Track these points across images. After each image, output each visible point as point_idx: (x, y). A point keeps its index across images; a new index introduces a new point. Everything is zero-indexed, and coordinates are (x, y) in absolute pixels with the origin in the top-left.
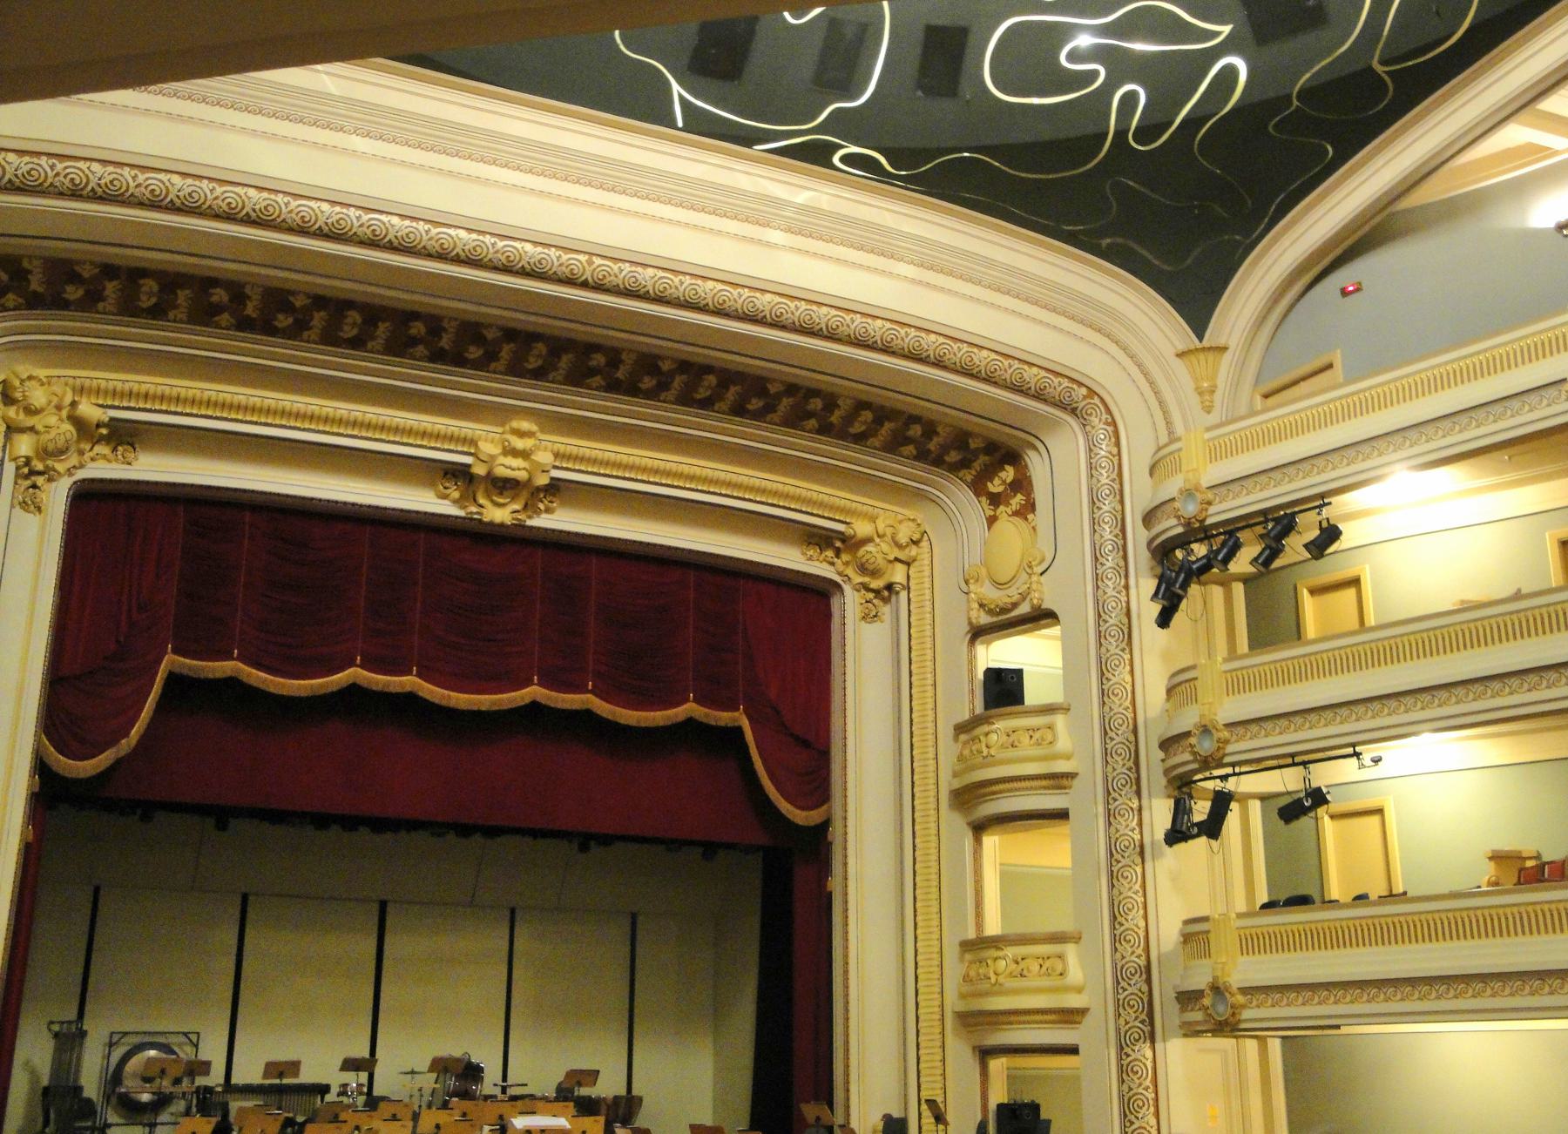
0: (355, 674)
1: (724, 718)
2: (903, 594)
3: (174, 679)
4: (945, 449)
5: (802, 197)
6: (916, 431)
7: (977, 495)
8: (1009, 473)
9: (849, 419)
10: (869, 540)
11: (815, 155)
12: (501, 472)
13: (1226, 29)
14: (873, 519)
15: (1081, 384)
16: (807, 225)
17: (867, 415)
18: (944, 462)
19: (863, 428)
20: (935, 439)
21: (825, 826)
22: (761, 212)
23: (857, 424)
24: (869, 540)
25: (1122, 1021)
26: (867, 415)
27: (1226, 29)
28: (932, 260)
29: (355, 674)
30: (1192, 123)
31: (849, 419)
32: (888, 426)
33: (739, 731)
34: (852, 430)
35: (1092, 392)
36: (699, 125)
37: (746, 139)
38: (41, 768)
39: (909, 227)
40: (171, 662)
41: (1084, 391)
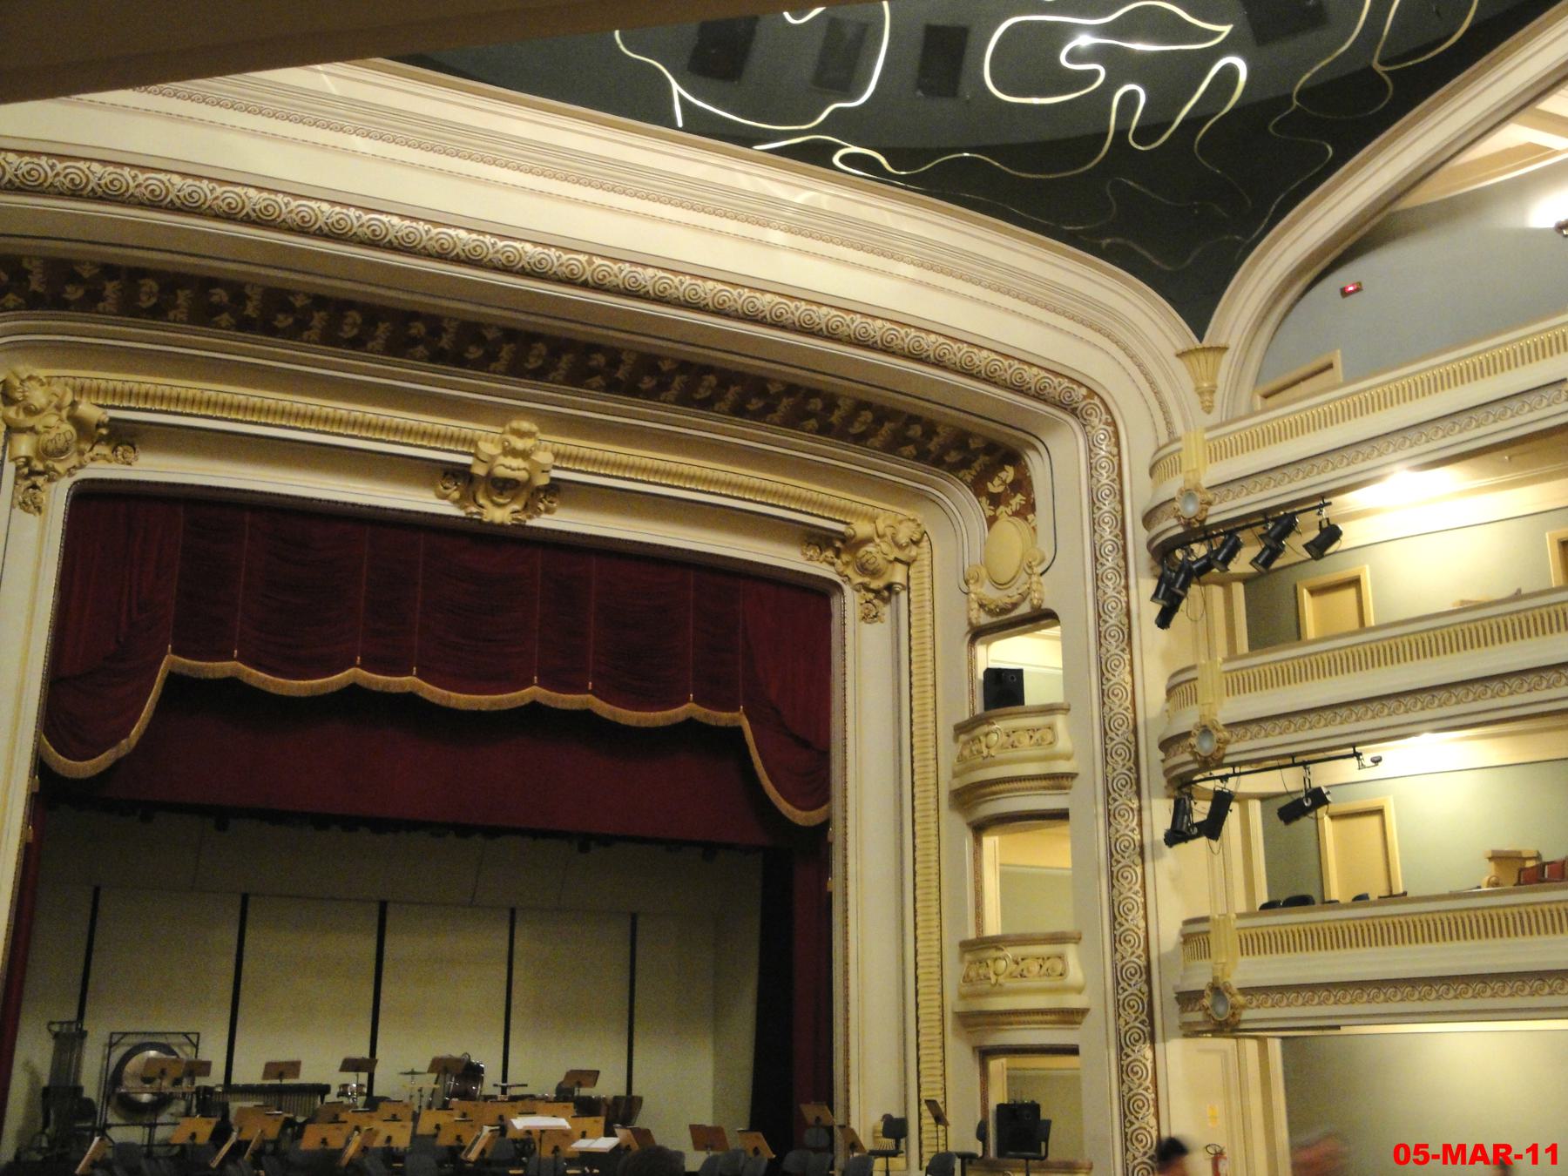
0: (355, 674)
1: (724, 718)
2: (903, 595)
3: (173, 679)
4: (945, 449)
5: (802, 197)
6: (916, 431)
7: (977, 495)
8: (1009, 474)
9: (850, 419)
10: (869, 540)
11: (815, 155)
12: (501, 472)
13: (1226, 29)
14: (873, 519)
15: (1081, 384)
16: (806, 225)
17: (867, 416)
18: (944, 462)
19: (863, 428)
20: (935, 439)
21: (826, 825)
22: (761, 213)
23: (857, 425)
24: (869, 540)
25: (1122, 1022)
26: (867, 416)
27: (1226, 29)
28: (933, 260)
29: (355, 674)
30: (1192, 122)
31: (850, 419)
32: (888, 426)
33: (739, 731)
34: (852, 431)
35: (1092, 393)
36: (699, 125)
37: (746, 138)
38: (41, 767)
39: (909, 226)
40: (171, 662)
41: (1084, 391)
